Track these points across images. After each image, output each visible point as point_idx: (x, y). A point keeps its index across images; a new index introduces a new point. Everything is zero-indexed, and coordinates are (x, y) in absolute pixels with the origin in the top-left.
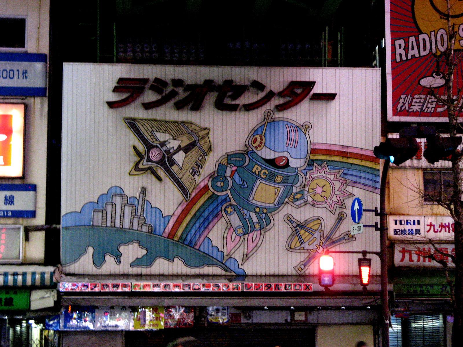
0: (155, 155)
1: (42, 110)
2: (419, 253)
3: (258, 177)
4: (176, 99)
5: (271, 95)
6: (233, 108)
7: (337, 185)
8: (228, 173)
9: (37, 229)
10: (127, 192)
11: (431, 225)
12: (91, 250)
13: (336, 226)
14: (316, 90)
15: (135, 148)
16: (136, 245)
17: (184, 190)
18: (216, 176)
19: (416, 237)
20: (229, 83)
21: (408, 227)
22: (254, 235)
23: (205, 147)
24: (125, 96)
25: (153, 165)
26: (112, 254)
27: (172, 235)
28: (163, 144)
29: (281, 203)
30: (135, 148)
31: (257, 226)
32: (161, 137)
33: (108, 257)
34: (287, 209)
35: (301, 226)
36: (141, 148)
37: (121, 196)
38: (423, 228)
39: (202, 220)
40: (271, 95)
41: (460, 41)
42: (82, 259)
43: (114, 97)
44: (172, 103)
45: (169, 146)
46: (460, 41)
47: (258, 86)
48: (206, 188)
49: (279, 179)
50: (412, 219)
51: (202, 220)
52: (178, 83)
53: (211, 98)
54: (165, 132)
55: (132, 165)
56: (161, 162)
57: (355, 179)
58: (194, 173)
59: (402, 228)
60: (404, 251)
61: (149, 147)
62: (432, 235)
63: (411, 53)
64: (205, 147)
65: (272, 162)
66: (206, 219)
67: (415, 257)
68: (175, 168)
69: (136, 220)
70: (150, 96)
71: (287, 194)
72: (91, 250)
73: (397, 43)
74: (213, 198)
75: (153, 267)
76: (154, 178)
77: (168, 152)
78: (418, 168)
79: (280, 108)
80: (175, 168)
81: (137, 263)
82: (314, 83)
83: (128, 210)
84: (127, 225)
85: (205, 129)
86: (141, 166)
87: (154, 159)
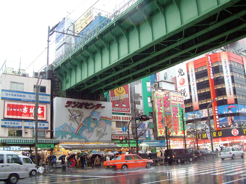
0: (73, 117)
1: (49, 106)
2: (116, 137)
3: (91, 122)
4: (77, 106)
5: (94, 106)
6: (88, 108)
7: (105, 124)
8: (86, 121)
9: (49, 131)
10: (68, 124)
11: (117, 131)
12: (61, 136)
13: (104, 132)
14: (102, 106)
15: (69, 115)
16: (69, 135)
17: (78, 124)
18: (84, 122)
19: (115, 134)
20: (87, 103)
21: (114, 132)
22: (91, 133)
23: (82, 116)
24: (68, 105)
25: (73, 119)
26: (65, 137)
27: (76, 133)
28: (75, 115)
29: (95, 127)
30: (69, 115)
31: (91, 131)
32: (74, 113)
33: (64, 137)
34: (96, 128)
35: (98, 132)
36: (71, 115)
37: (67, 125)
38: (116, 132)
39: (81, 130)
40: (94, 106)
41: (5, 102)
42: (59, 138)
43: (66, 105)
44: (77, 106)
45: (76, 115)
46: (5, 102)
47: (92, 104)
48: (82, 124)
49: (95, 122)
50: (114, 130)
51: (81, 130)
52: (78, 103)
53: (84, 106)
54: (75, 112)
55: (69, 119)
56: (74, 118)
57: (107, 123)
58: (80, 121)
59: (113, 132)
60: (114, 136)
61: (72, 115)
62: (117, 133)
63: (114, 100)
64: (82, 116)
65: (94, 119)
66: (82, 130)
67: (115, 137)
68: (77, 120)
69: (69, 130)
70: (73, 105)
71: (96, 125)
72: (61, 136)
73: (111, 97)
74: (83, 126)
75: (72, 139)
76: (73, 122)
77: (75, 116)
78: (115, 121)
79: (96, 109)
80: (77, 120)
81: (69, 139)
82: (101, 104)
83: (68, 127)
84: (68, 131)
85: (82, 112)
86: (70, 119)
87: (73, 118)
